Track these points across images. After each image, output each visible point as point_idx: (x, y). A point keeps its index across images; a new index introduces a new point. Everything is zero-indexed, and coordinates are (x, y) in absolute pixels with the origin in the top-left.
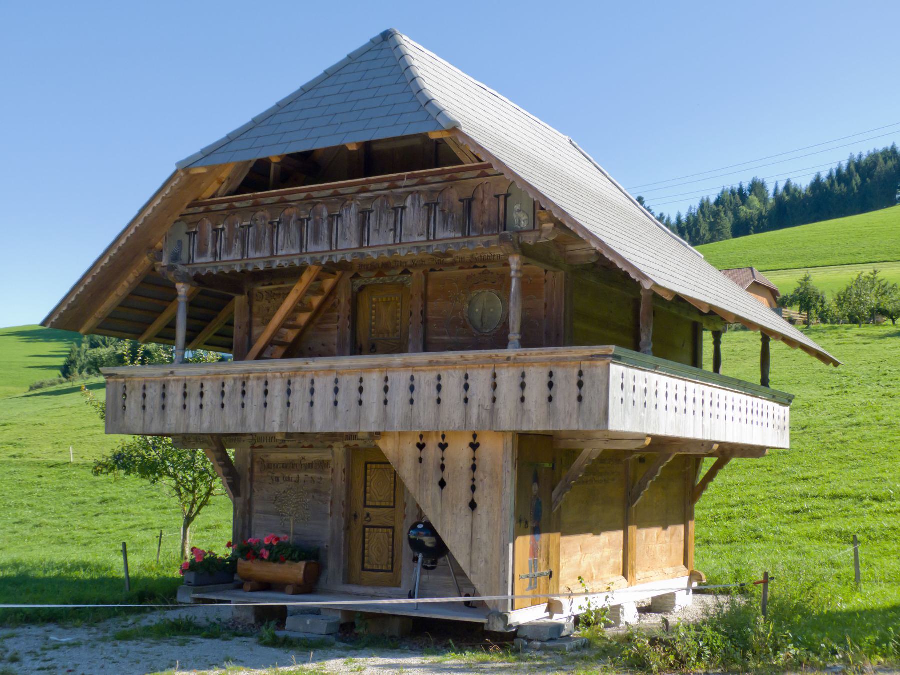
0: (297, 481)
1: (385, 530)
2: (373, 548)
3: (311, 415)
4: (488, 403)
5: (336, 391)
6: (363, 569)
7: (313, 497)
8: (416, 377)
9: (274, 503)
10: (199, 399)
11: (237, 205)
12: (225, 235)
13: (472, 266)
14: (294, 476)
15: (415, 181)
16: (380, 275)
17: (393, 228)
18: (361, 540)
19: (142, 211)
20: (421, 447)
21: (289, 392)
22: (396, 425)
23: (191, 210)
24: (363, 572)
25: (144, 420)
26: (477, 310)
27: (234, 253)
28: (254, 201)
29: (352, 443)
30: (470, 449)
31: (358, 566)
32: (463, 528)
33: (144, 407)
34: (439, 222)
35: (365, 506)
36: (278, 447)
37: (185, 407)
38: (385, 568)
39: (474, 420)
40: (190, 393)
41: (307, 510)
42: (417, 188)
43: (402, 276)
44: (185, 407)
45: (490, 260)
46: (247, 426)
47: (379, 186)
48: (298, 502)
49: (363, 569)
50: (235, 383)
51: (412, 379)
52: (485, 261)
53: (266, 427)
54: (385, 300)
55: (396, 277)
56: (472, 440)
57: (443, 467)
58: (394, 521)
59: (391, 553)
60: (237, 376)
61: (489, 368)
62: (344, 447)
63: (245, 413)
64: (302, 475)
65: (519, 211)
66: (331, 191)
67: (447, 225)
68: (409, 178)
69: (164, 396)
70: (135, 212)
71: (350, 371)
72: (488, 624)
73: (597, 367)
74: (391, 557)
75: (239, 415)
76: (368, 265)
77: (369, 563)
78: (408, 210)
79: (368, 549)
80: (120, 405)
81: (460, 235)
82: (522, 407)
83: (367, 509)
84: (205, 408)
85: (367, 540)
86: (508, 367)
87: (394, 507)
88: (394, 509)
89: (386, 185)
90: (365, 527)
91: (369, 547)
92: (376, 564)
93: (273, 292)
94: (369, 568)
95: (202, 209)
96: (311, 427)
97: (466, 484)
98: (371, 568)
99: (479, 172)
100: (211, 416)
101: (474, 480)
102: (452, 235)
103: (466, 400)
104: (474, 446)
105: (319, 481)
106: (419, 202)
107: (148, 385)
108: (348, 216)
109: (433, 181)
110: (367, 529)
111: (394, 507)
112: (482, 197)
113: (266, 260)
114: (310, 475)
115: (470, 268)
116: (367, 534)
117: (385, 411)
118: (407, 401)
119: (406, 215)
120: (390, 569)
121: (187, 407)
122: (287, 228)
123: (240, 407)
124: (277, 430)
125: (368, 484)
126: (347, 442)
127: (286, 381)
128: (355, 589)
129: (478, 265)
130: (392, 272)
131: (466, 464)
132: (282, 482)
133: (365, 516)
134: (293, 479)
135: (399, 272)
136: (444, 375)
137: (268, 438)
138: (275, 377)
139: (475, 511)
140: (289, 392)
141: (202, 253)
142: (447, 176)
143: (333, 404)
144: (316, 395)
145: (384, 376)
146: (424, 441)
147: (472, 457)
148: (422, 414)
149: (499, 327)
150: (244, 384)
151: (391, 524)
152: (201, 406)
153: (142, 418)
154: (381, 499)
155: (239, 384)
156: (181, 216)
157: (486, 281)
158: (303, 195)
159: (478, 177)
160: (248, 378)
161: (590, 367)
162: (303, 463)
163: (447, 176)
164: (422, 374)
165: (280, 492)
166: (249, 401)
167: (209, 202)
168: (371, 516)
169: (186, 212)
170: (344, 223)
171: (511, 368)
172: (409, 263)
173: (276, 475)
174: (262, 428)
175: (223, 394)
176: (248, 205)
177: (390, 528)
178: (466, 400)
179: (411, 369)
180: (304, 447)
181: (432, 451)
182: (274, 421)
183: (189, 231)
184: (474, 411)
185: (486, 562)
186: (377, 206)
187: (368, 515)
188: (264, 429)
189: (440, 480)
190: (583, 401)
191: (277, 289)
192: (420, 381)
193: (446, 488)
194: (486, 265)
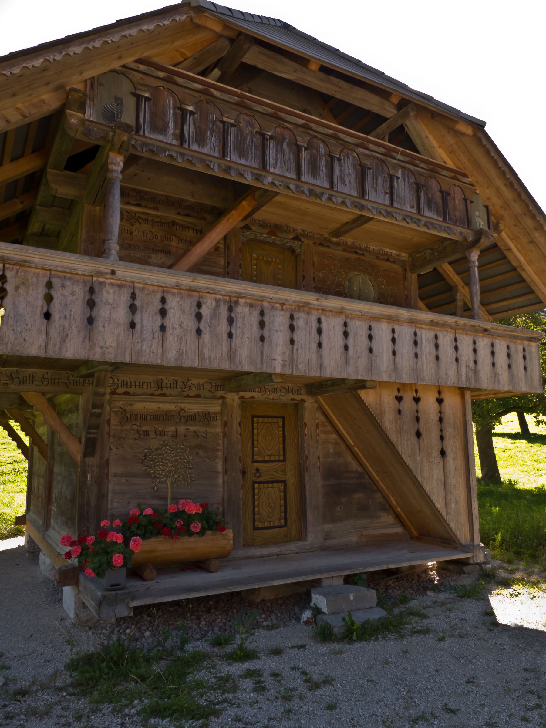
0: (176, 435)
1: (276, 485)
2: (264, 504)
3: (320, 357)
4: (472, 364)
6: (255, 528)
7: (198, 453)
8: (418, 333)
9: (142, 463)
10: (159, 318)
11: (216, 93)
13: (353, 251)
14: (171, 429)
15: (407, 159)
16: (272, 233)
18: (251, 497)
20: (399, 399)
22: (404, 376)
23: (142, 67)
24: (255, 531)
25: (47, 334)
26: (355, 288)
27: (208, 147)
28: (240, 99)
30: (437, 403)
32: (437, 473)
33: (47, 316)
35: (254, 461)
36: (152, 395)
37: (132, 325)
38: (277, 524)
40: (142, 307)
41: (190, 468)
42: (407, 165)
43: (294, 241)
44: (132, 325)
45: (367, 250)
46: (237, 362)
47: (375, 148)
48: (177, 460)
49: (255, 528)
50: (217, 306)
51: (415, 334)
52: (362, 249)
54: (265, 259)
55: (288, 241)
56: (437, 396)
57: (418, 419)
58: (285, 474)
59: (283, 508)
60: (221, 297)
61: (471, 335)
62: (239, 399)
63: (233, 344)
64: (182, 429)
66: (331, 132)
68: (403, 154)
69: (91, 304)
71: (361, 316)
72: (473, 557)
73: (532, 346)
74: (283, 510)
75: (224, 346)
76: (260, 221)
79: (258, 507)
82: (494, 370)
83: (256, 465)
84: (169, 331)
85: (256, 497)
86: (483, 336)
87: (284, 460)
88: (284, 463)
89: (383, 150)
91: (259, 504)
93: (137, 215)
94: (260, 526)
95: (161, 74)
96: (321, 371)
97: (435, 435)
98: (263, 526)
99: (452, 174)
104: (440, 401)
105: (204, 435)
107: (55, 281)
108: (346, 163)
110: (256, 485)
113: (255, 171)
114: (192, 429)
115: (351, 252)
116: (256, 491)
117: (394, 361)
118: (412, 354)
120: (283, 524)
121: (138, 327)
122: (279, 147)
123: (225, 336)
125: (255, 438)
127: (288, 314)
129: (358, 251)
130: (284, 235)
131: (434, 416)
132: (154, 436)
133: (254, 471)
135: (291, 237)
136: (440, 334)
137: (137, 383)
138: (273, 308)
142: (431, 167)
143: (343, 349)
145: (391, 327)
146: (401, 394)
148: (425, 368)
150: (230, 309)
152: (163, 328)
153: (44, 332)
154: (269, 453)
155: (224, 311)
156: (124, 66)
157: (360, 266)
158: (301, 122)
160: (237, 303)
161: (529, 346)
162: (182, 414)
163: (431, 167)
164: (423, 331)
165: (151, 449)
166: (239, 331)
168: (261, 471)
169: (133, 65)
171: (484, 338)
172: (300, 231)
173: (145, 428)
174: (259, 366)
175: (199, 316)
179: (413, 325)
180: (188, 396)
181: (408, 403)
182: (274, 360)
184: (463, 370)
187: (258, 470)
188: (261, 368)
189: (416, 430)
191: (144, 213)
192: (421, 337)
193: (421, 438)
194: (365, 253)
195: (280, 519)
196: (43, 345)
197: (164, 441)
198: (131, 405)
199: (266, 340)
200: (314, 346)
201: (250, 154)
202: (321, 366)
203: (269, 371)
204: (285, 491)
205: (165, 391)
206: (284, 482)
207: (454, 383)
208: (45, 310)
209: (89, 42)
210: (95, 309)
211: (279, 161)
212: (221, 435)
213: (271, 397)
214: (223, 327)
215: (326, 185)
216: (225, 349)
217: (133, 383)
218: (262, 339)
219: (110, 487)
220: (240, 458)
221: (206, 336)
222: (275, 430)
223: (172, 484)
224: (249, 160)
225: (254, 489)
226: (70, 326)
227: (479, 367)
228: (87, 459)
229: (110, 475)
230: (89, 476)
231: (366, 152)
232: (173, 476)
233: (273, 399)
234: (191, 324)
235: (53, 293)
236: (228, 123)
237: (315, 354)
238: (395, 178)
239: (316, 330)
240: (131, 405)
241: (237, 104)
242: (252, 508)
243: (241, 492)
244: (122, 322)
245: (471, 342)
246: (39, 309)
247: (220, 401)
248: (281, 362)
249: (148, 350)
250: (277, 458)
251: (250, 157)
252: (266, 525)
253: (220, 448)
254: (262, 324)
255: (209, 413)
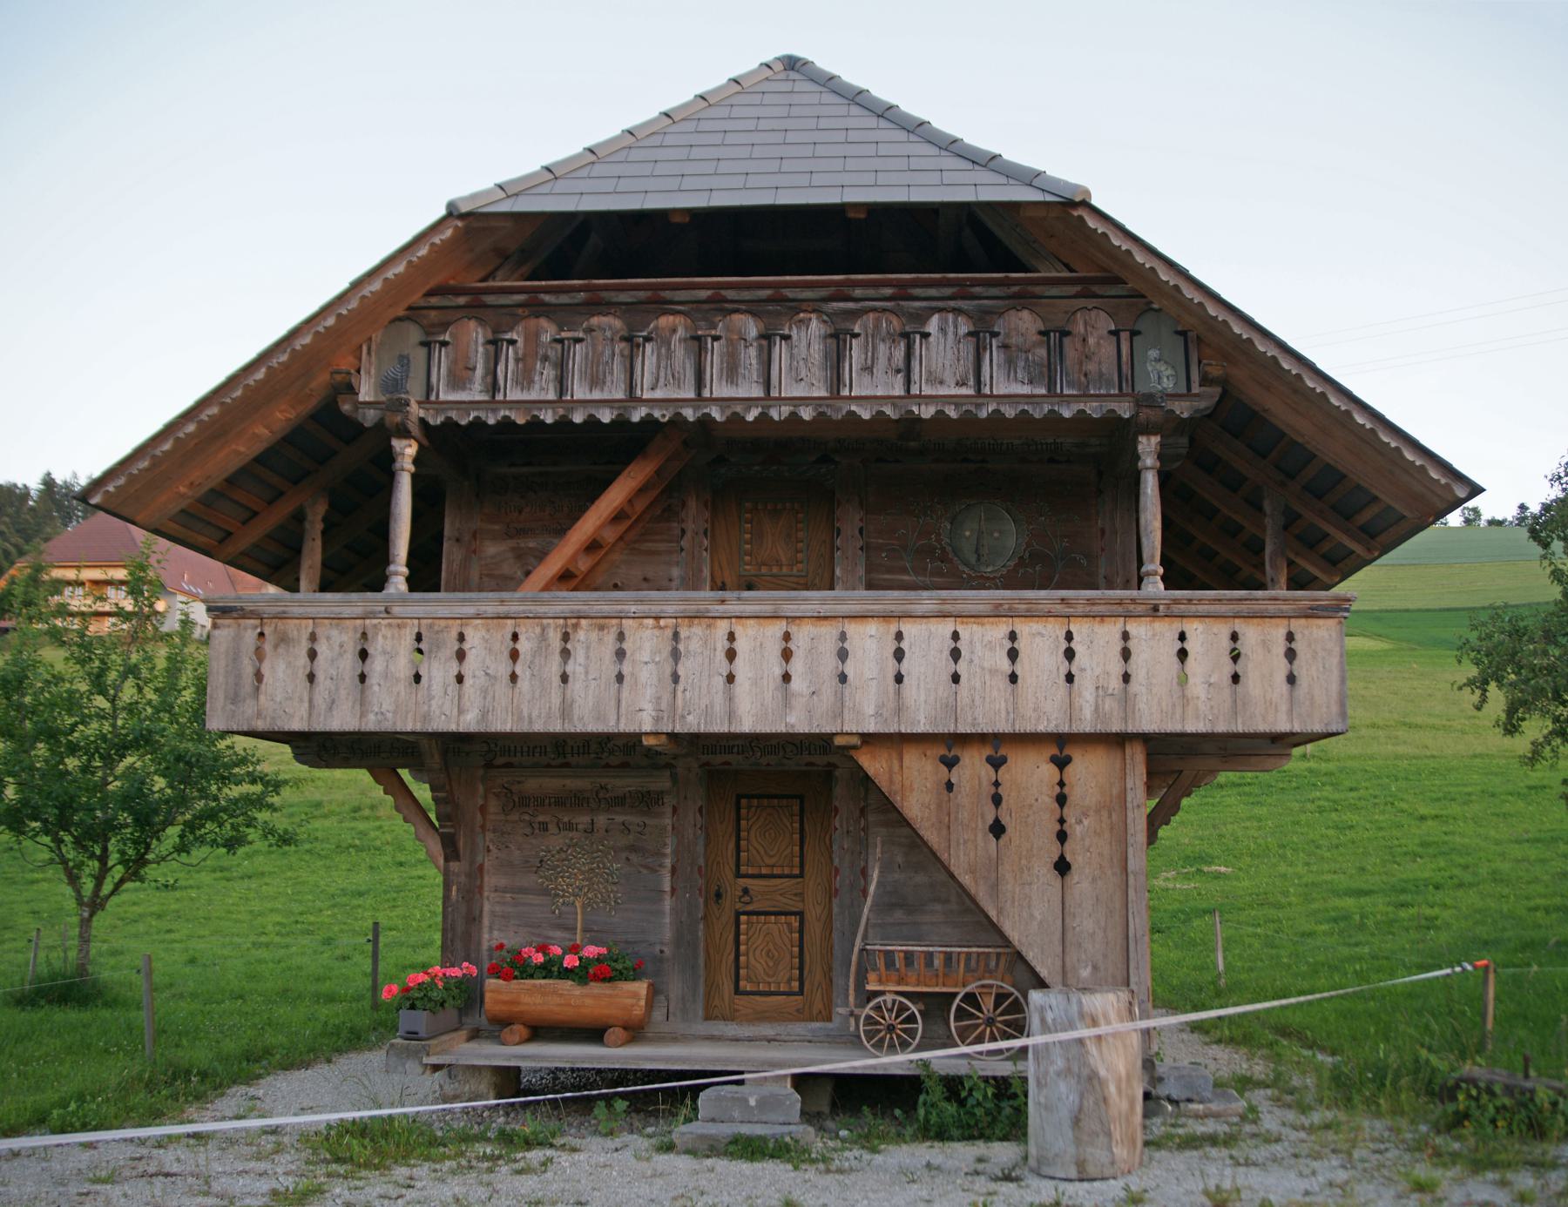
2: (758, 952)
4: (1115, 683)
5: (787, 655)
6: (737, 991)
7: (628, 859)
11: (547, 298)
12: (516, 353)
15: (948, 291)
17: (901, 365)
18: (731, 937)
19: (357, 285)
21: (676, 655)
23: (434, 301)
25: (311, 701)
27: (537, 386)
29: (718, 759)
31: (727, 987)
34: (999, 366)
35: (738, 875)
36: (549, 766)
39: (1088, 713)
41: (615, 884)
42: (952, 304)
53: (623, 720)
63: (568, 692)
65: (1158, 360)
66: (768, 292)
67: (1016, 372)
70: (343, 285)
77: (748, 979)
78: (931, 339)
79: (747, 954)
80: (248, 670)
81: (1043, 391)
83: (742, 882)
84: (468, 681)
85: (742, 937)
87: (801, 875)
89: (888, 291)
90: (738, 914)
92: (764, 982)
95: (462, 300)
98: (755, 989)
100: (485, 698)
101: (1062, 821)
102: (1026, 390)
103: (1070, 678)
106: (956, 327)
109: (985, 295)
110: (743, 918)
111: (801, 875)
112: (1082, 330)
116: (743, 927)
118: (947, 678)
119: (927, 349)
121: (424, 680)
122: (663, 351)
123: (556, 680)
124: (647, 727)
126: (705, 758)
128: (731, 1029)
134: (580, 827)
137: (525, 749)
139: (1068, 878)
140: (676, 655)
141: (458, 380)
142: (1015, 289)
144: (738, 661)
147: (1057, 779)
149: (1012, 563)
151: (798, 907)
152: (460, 679)
153: (306, 698)
154: (773, 861)
156: (410, 308)
158: (704, 294)
159: (1075, 296)
163: (1015, 289)
167: (480, 288)
168: (751, 892)
169: (422, 303)
170: (795, 351)
173: (541, 818)
175: (514, 655)
176: (576, 301)
177: (795, 914)
178: (1070, 678)
180: (607, 766)
183: (429, 339)
185: (1095, 968)
186: (865, 328)
187: (746, 891)
190: (1298, 682)
195: (790, 980)
196: (305, 716)
197: (572, 839)
198: (519, 782)
199: (627, 680)
200: (719, 681)
201: (609, 378)
202: (731, 715)
203: (631, 728)
204: (801, 931)
205: (569, 759)
206: (800, 914)
207: (1056, 726)
208: (308, 671)
209: (318, 325)
210: (368, 661)
211: (662, 374)
212: (670, 828)
213: (764, 761)
214: (554, 666)
215: (757, 392)
216: (556, 700)
217: (519, 749)
218: (620, 678)
219: (487, 907)
220: (700, 867)
221: (524, 684)
222: (785, 820)
223: (584, 907)
224: (606, 388)
225: (737, 924)
226: (337, 689)
227: (1134, 686)
228: (451, 864)
229: (486, 888)
230: (454, 888)
231: (850, 305)
232: (585, 894)
233: (768, 765)
234: (503, 668)
235: (317, 648)
236: (568, 339)
237: (721, 693)
238: (918, 337)
239: (723, 654)
240: (519, 782)
241: (586, 303)
242: (732, 956)
243: (701, 926)
244: (402, 676)
245: (1118, 636)
246: (301, 671)
247: (668, 773)
248: (654, 714)
249: (437, 713)
250: (787, 871)
251: (608, 384)
252: (762, 987)
253: (668, 851)
254: (620, 654)
255: (649, 792)
